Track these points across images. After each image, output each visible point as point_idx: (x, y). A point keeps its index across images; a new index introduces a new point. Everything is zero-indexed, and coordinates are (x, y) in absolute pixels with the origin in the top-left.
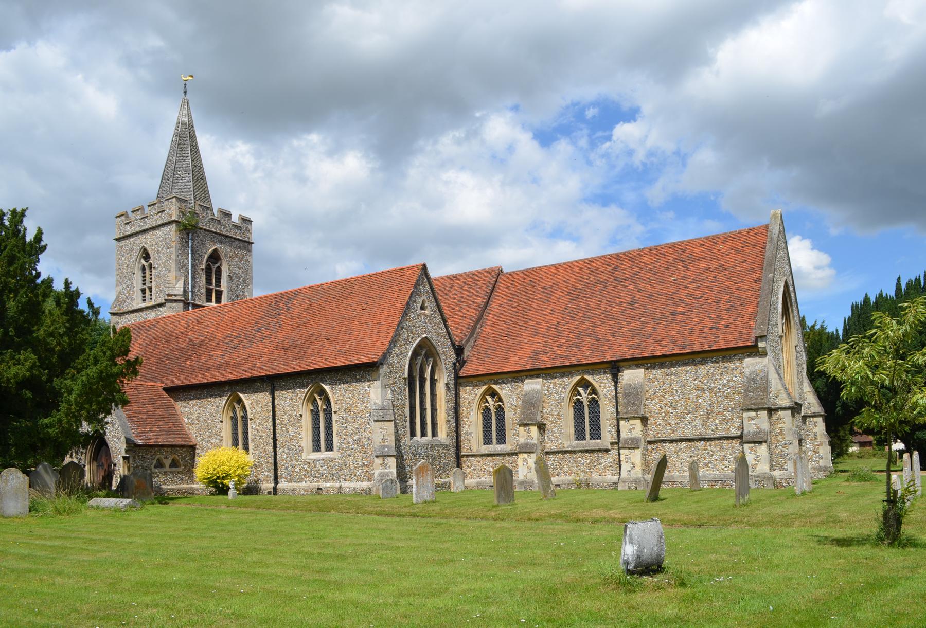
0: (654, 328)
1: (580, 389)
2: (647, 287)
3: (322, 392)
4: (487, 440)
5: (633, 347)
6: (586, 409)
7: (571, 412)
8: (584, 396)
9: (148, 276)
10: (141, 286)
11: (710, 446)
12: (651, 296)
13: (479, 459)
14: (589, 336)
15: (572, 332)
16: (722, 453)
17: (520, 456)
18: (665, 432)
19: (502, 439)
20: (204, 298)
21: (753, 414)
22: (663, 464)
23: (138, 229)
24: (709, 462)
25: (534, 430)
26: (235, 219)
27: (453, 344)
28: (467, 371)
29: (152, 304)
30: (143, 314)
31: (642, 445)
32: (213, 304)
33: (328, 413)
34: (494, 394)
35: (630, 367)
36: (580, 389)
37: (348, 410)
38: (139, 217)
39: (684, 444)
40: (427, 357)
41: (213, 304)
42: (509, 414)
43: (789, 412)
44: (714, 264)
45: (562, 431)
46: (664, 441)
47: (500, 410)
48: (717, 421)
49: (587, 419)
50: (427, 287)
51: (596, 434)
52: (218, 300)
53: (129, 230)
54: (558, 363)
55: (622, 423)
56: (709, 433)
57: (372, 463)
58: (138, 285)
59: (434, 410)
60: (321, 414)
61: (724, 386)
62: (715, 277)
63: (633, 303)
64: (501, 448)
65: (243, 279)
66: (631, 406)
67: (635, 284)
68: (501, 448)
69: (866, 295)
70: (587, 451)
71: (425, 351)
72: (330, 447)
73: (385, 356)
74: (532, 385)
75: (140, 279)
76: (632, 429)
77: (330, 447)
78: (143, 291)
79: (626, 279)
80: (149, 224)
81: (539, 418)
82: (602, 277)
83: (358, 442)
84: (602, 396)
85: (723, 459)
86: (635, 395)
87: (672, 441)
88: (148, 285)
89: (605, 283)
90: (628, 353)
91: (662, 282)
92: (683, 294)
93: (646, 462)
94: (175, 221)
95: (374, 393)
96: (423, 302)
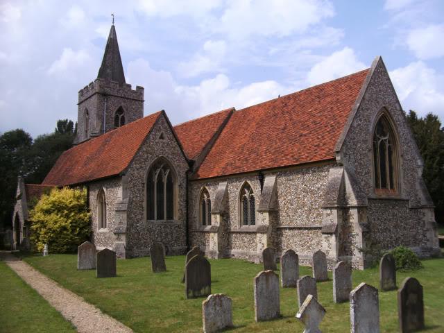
5: (272, 160)
11: (311, 234)
16: (317, 240)
17: (258, 235)
21: (329, 211)
26: (134, 88)
27: (186, 159)
35: (269, 175)
39: (296, 231)
40: (165, 168)
43: (356, 210)
48: (315, 215)
56: (310, 225)
61: (318, 189)
67: (291, 115)
69: (381, 58)
73: (126, 169)
74: (222, 187)
90: (269, 164)
94: (98, 93)
96: (162, 135)
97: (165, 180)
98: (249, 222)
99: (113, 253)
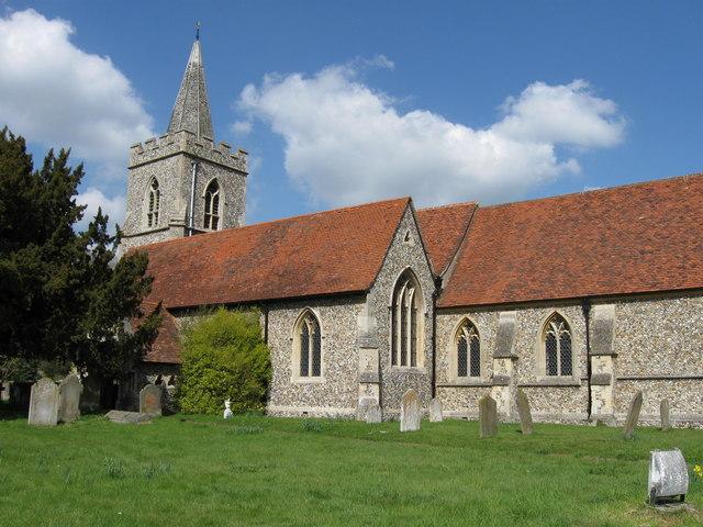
0: (624, 266)
1: (553, 324)
2: (617, 226)
3: (313, 317)
4: (462, 372)
6: (558, 343)
7: (543, 347)
8: (557, 332)
9: (155, 203)
10: (148, 212)
11: (678, 386)
12: (620, 234)
13: (454, 390)
14: (562, 272)
15: (544, 267)
16: (690, 394)
17: (494, 388)
18: (634, 370)
19: (476, 372)
20: (202, 224)
22: (638, 402)
23: (150, 159)
24: (677, 402)
25: (508, 362)
28: (443, 301)
29: (157, 228)
30: (148, 237)
31: (612, 381)
32: (210, 230)
33: (317, 337)
34: (469, 325)
36: (553, 324)
37: (336, 336)
38: (151, 148)
39: (653, 383)
40: (409, 287)
41: (210, 230)
42: (483, 347)
44: (680, 206)
45: (536, 366)
46: (633, 379)
47: (476, 343)
49: (558, 353)
50: (412, 219)
51: (567, 370)
52: (214, 227)
53: (142, 160)
54: (532, 297)
55: (593, 359)
57: (357, 389)
58: (146, 210)
59: (414, 339)
60: (310, 339)
61: (692, 325)
62: (681, 218)
63: (603, 240)
64: (474, 380)
65: (235, 208)
66: (600, 341)
68: (474, 380)
70: (558, 386)
71: (407, 278)
72: (317, 372)
74: (507, 317)
75: (148, 204)
76: (602, 366)
77: (317, 372)
78: (150, 216)
79: (597, 217)
80: (160, 154)
81: (513, 351)
82: (573, 214)
83: (344, 368)
84: (573, 332)
85: (690, 400)
86: (604, 331)
87: (641, 379)
88: (154, 211)
89: (576, 220)
91: (631, 221)
92: (651, 233)
93: (616, 401)
94: (185, 153)
95: (362, 319)
97: (408, 304)
98: (469, 373)
99: (27, 417)
